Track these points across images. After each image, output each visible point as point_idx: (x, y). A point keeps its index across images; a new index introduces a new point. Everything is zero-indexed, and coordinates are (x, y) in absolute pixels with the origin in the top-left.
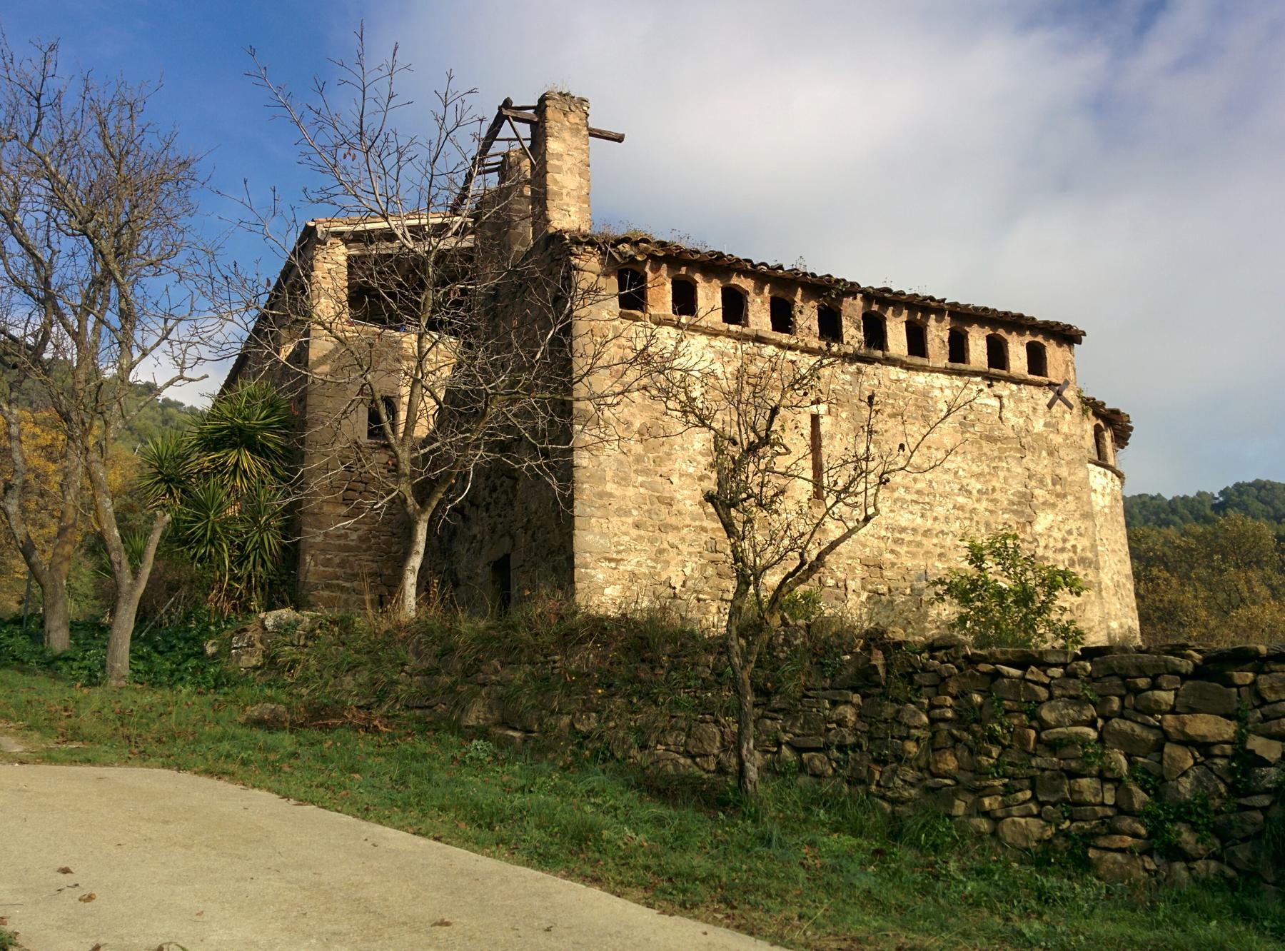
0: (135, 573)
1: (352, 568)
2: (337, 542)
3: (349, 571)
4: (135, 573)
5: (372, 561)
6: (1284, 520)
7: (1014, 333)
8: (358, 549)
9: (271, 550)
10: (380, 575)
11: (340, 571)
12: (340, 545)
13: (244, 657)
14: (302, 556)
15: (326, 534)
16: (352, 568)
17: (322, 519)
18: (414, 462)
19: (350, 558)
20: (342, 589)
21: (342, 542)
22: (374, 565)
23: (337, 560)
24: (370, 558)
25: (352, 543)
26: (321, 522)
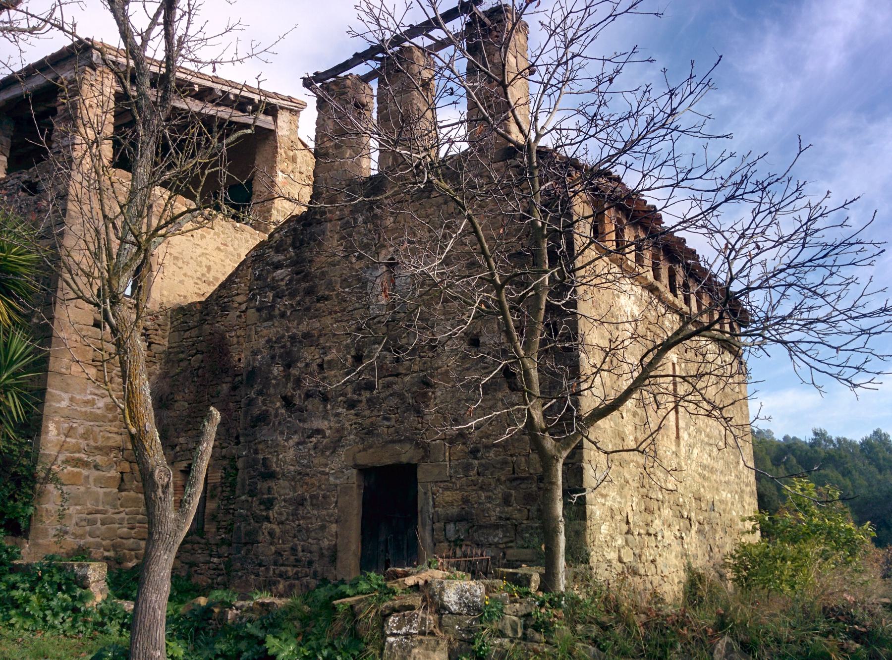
0: (180, 504)
1: (96, 441)
2: (83, 409)
3: (92, 443)
4: (180, 504)
5: (117, 433)
6: (192, 3)
7: (767, 22)
8: (102, 418)
9: (17, 412)
10: (123, 450)
11: (83, 443)
12: (86, 412)
13: (415, 651)
14: (44, 423)
15: (72, 399)
16: (96, 441)
17: (69, 381)
18: (544, 414)
19: (95, 429)
20: (86, 464)
21: (88, 409)
22: (118, 438)
23: (81, 430)
24: (116, 430)
25: (99, 412)
26: (68, 384)
